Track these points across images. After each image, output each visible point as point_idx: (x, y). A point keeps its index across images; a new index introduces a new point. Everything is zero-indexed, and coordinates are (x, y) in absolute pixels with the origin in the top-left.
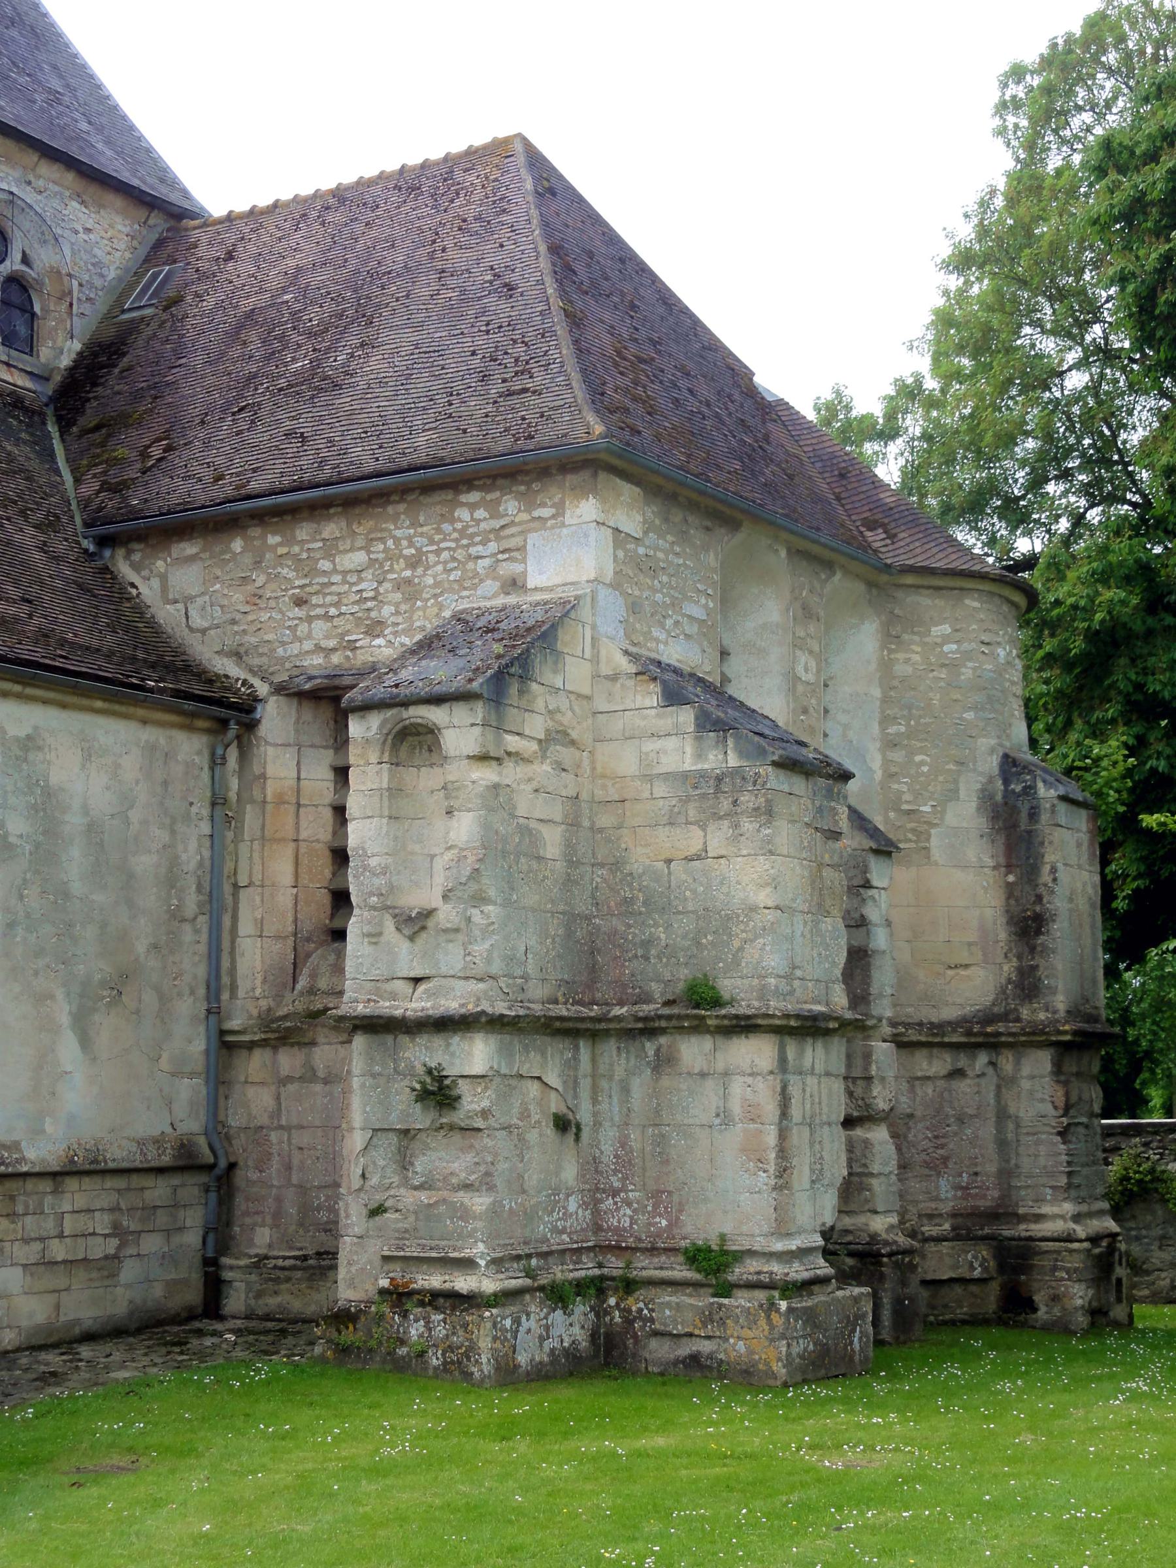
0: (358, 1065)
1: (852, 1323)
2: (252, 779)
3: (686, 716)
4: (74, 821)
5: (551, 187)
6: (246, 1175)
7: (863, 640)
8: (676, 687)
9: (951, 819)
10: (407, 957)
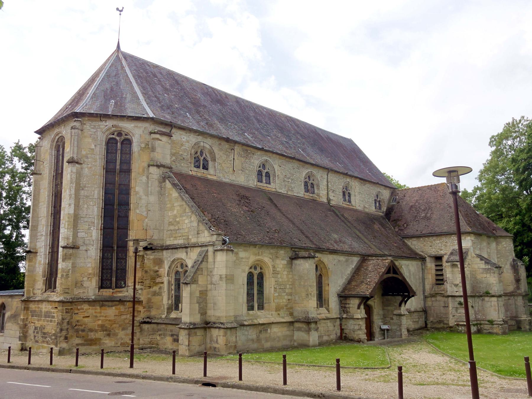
1: (506, 328)
3: (483, 262)
6: (429, 312)
7: (494, 245)
8: (482, 258)
9: (506, 267)
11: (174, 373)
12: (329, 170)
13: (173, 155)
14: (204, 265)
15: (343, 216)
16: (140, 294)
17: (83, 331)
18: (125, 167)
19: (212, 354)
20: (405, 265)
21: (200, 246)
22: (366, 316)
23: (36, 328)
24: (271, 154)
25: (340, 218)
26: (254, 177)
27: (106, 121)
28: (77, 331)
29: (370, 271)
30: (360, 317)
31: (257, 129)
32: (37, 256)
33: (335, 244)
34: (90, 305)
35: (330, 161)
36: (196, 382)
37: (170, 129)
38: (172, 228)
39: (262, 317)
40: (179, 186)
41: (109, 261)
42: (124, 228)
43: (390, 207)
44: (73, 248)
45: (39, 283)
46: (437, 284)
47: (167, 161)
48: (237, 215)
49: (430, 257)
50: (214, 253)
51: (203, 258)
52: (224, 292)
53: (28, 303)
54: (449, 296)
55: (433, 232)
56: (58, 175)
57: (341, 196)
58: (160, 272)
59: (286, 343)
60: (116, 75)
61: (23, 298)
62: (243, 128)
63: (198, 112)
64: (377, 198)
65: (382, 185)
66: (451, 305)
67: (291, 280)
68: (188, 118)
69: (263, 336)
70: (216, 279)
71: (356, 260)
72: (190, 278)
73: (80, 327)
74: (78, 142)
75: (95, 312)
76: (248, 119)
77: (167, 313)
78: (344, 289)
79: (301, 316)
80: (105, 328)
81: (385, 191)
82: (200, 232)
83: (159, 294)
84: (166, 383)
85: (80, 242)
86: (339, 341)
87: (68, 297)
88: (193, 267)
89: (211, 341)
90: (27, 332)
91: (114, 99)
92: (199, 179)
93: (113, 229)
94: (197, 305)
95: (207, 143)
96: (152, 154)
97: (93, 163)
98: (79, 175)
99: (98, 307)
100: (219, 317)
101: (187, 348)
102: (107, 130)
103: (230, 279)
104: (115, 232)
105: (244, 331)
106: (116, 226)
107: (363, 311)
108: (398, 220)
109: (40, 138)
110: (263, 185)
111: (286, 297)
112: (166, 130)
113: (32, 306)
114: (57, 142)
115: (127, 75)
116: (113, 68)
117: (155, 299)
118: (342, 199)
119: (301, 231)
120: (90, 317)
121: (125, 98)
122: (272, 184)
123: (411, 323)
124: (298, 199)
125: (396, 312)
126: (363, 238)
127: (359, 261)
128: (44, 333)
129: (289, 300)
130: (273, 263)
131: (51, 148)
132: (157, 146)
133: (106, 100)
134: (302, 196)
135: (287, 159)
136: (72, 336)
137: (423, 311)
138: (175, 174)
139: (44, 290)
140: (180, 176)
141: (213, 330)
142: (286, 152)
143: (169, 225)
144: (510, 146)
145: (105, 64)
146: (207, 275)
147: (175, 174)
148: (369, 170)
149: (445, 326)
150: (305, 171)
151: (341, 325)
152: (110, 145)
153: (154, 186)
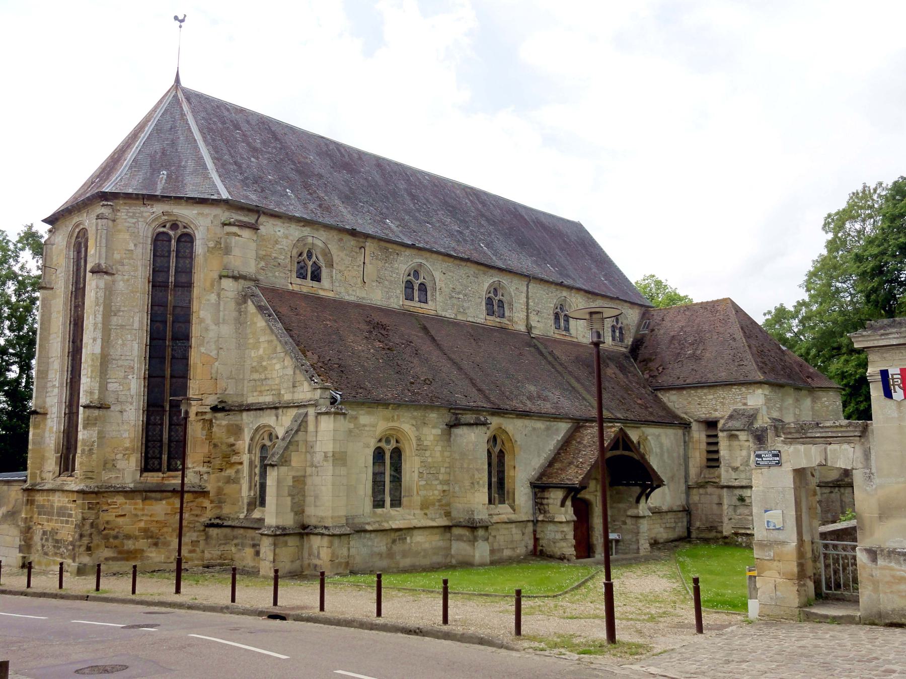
0: (725, 494)
2: (691, 438)
4: (665, 448)
5: (738, 310)
6: (694, 512)
7: (808, 402)
10: (734, 475)
11: (233, 600)
12: (529, 278)
13: (259, 258)
14: (300, 436)
15: (551, 353)
16: (206, 481)
17: (116, 537)
18: (183, 279)
19: (311, 575)
20: (654, 435)
21: (297, 406)
22: (575, 518)
23: (44, 533)
24: (428, 255)
25: (545, 358)
26: (398, 291)
28: (106, 538)
29: (585, 446)
30: (564, 520)
31: (408, 212)
32: (46, 419)
33: (528, 402)
34: (126, 498)
35: (536, 262)
36: (260, 613)
37: (256, 217)
38: (256, 376)
39: (397, 518)
40: (267, 309)
42: (182, 376)
43: (639, 337)
44: (100, 408)
45: (49, 461)
46: (708, 467)
47: (251, 268)
48: (362, 358)
50: (316, 417)
51: (300, 425)
52: (329, 479)
53: (33, 494)
54: (723, 487)
55: (703, 380)
56: (78, 292)
57: (551, 321)
58: (237, 446)
59: (438, 559)
60: (171, 128)
61: (25, 486)
62: (384, 210)
63: (307, 186)
64: (617, 322)
65: (626, 301)
66: (726, 502)
68: (289, 197)
69: (398, 547)
70: (318, 458)
71: (563, 427)
72: (277, 457)
73: (112, 532)
74: (107, 240)
75: (135, 509)
76: (394, 194)
77: (248, 511)
78: (542, 475)
79: (462, 517)
80: (149, 534)
81: (630, 311)
82: (297, 384)
83: (236, 481)
84: (219, 614)
85: (110, 399)
86: (530, 558)
87: (92, 485)
88: (283, 439)
89: (310, 555)
90: (31, 538)
91: (167, 169)
92: (306, 297)
93: (164, 377)
94: (289, 499)
95: (319, 239)
96: (226, 259)
98: (109, 292)
99: (140, 501)
100: (322, 518)
101: (271, 565)
102: (154, 220)
103: (339, 458)
104: (168, 383)
105: (365, 541)
106: (168, 373)
107: (571, 510)
108: (651, 360)
109: (50, 231)
110: (415, 305)
111: (440, 487)
113: (40, 498)
114: (77, 237)
115: (189, 128)
116: (168, 117)
117: (229, 489)
118: (553, 326)
119: (471, 379)
120: (127, 516)
121: (185, 167)
122: (430, 302)
123: (662, 530)
124: (475, 326)
125: (630, 512)
126: (581, 390)
127: (570, 428)
128: (57, 541)
129: (444, 491)
130: (417, 433)
131: (68, 246)
132: (233, 244)
133: (154, 170)
134: (483, 321)
135: (457, 262)
136: (98, 546)
137: (684, 510)
138: (264, 290)
140: (273, 293)
141: (312, 537)
142: (455, 250)
143: (252, 372)
144: (859, 232)
145: (154, 110)
146: (306, 452)
147: (264, 290)
148: (605, 276)
149: (719, 535)
150: (487, 281)
151: (535, 532)
152: (159, 243)
153: (229, 308)
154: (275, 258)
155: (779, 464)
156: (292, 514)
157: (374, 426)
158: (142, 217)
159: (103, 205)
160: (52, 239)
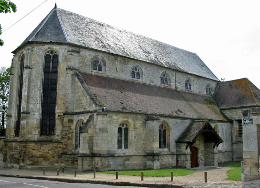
4: (224, 130)
13: (80, 63)
17: (32, 157)
18: (54, 70)
22: (191, 153)
23: (10, 155)
27: (45, 46)
34: (35, 144)
37: (79, 49)
38: (78, 103)
41: (46, 121)
42: (54, 103)
47: (77, 66)
49: (236, 120)
56: (22, 75)
64: (208, 87)
67: (145, 132)
71: (188, 122)
81: (213, 83)
85: (30, 111)
97: (38, 68)
98: (30, 75)
102: (45, 50)
105: (115, 159)
109: (14, 56)
112: (77, 49)
122: (141, 79)
125: (211, 151)
129: (144, 143)
131: (19, 61)
134: (160, 85)
139: (14, 136)
140: (84, 74)
150: (161, 72)
151: (177, 158)
154: (86, 63)
155: (252, 123)
156: (89, 150)
157: (118, 119)
158: (41, 49)
159: (29, 46)
160: (14, 58)
